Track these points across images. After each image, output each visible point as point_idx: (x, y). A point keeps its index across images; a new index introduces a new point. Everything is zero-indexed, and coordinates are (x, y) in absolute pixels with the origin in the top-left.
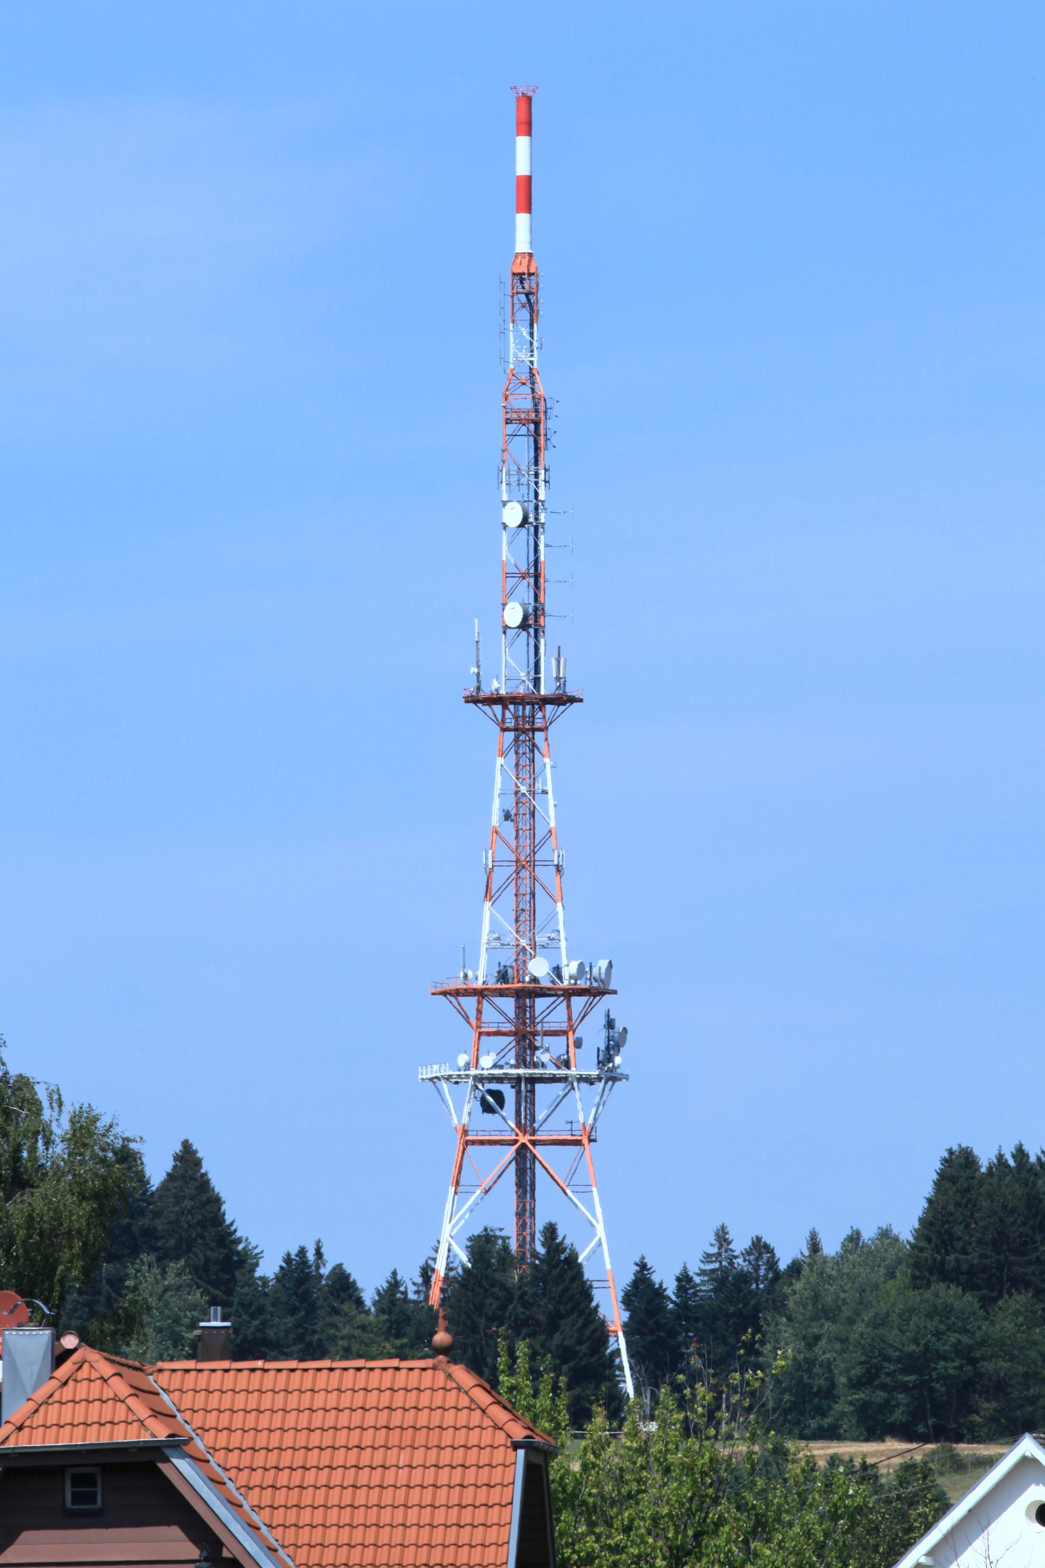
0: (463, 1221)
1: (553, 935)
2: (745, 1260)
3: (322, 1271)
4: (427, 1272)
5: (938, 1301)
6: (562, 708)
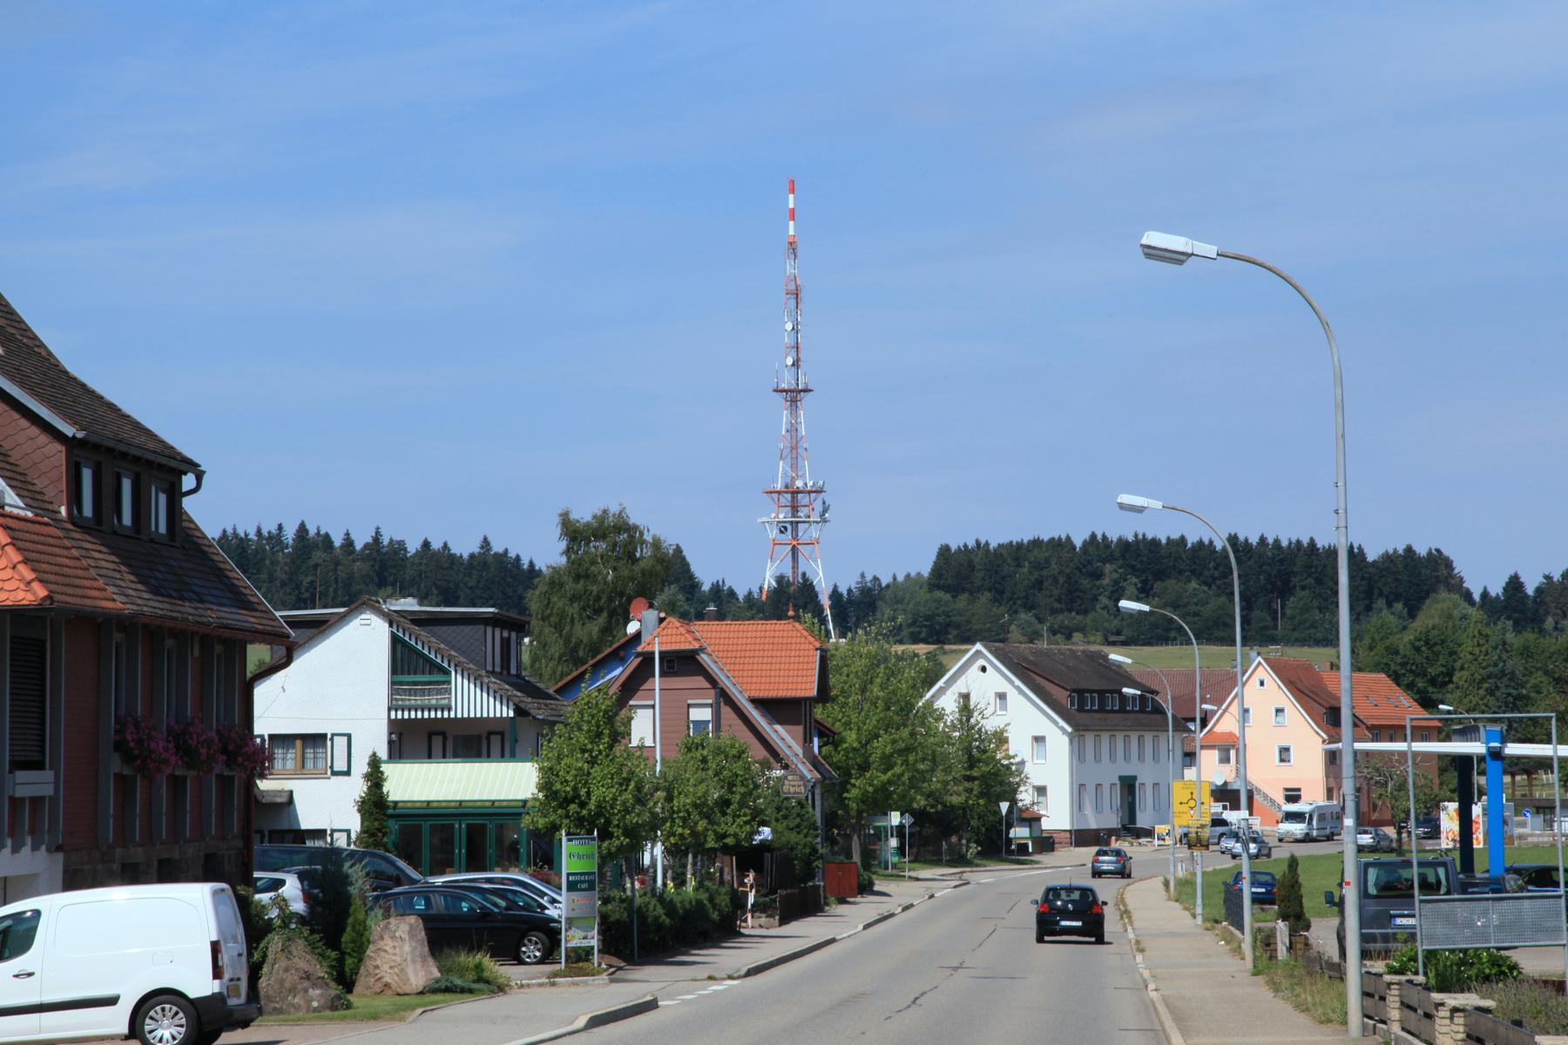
4: (761, 589)
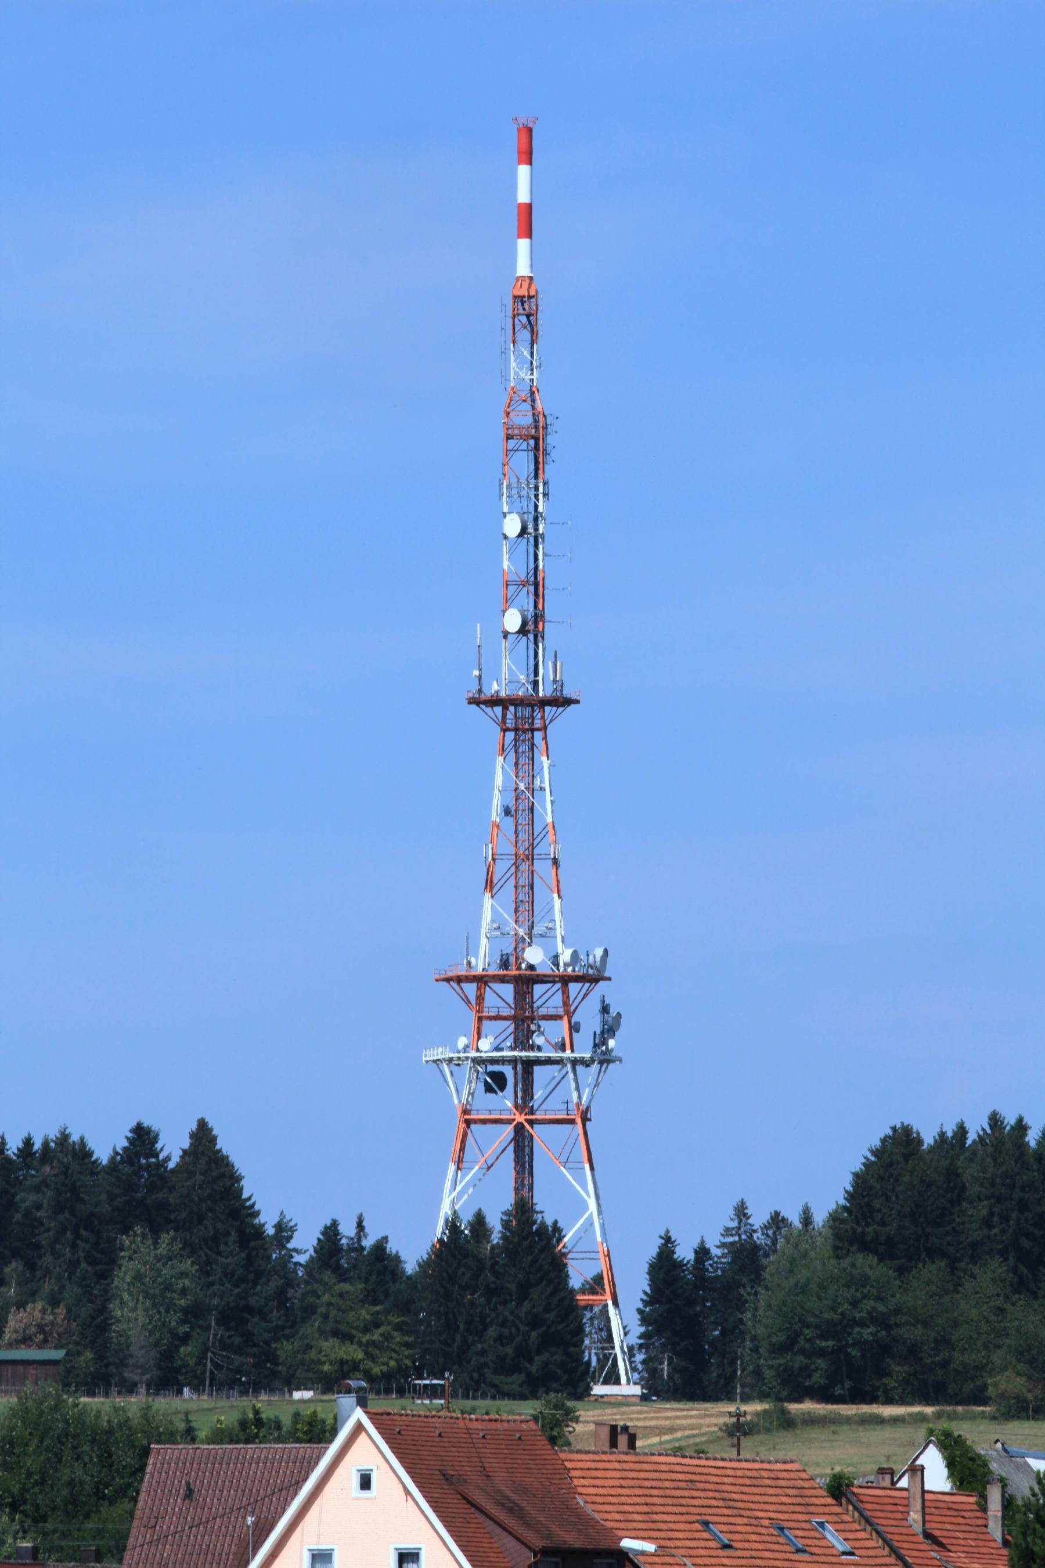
0: (466, 1197)
1: (550, 925)
2: (763, 1234)
3: (364, 1243)
5: (854, 1271)
6: (561, 709)
